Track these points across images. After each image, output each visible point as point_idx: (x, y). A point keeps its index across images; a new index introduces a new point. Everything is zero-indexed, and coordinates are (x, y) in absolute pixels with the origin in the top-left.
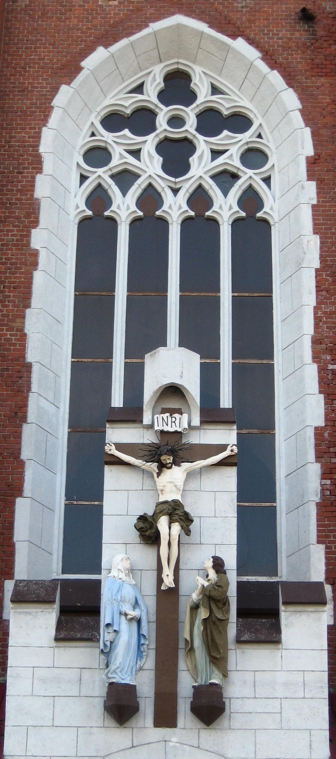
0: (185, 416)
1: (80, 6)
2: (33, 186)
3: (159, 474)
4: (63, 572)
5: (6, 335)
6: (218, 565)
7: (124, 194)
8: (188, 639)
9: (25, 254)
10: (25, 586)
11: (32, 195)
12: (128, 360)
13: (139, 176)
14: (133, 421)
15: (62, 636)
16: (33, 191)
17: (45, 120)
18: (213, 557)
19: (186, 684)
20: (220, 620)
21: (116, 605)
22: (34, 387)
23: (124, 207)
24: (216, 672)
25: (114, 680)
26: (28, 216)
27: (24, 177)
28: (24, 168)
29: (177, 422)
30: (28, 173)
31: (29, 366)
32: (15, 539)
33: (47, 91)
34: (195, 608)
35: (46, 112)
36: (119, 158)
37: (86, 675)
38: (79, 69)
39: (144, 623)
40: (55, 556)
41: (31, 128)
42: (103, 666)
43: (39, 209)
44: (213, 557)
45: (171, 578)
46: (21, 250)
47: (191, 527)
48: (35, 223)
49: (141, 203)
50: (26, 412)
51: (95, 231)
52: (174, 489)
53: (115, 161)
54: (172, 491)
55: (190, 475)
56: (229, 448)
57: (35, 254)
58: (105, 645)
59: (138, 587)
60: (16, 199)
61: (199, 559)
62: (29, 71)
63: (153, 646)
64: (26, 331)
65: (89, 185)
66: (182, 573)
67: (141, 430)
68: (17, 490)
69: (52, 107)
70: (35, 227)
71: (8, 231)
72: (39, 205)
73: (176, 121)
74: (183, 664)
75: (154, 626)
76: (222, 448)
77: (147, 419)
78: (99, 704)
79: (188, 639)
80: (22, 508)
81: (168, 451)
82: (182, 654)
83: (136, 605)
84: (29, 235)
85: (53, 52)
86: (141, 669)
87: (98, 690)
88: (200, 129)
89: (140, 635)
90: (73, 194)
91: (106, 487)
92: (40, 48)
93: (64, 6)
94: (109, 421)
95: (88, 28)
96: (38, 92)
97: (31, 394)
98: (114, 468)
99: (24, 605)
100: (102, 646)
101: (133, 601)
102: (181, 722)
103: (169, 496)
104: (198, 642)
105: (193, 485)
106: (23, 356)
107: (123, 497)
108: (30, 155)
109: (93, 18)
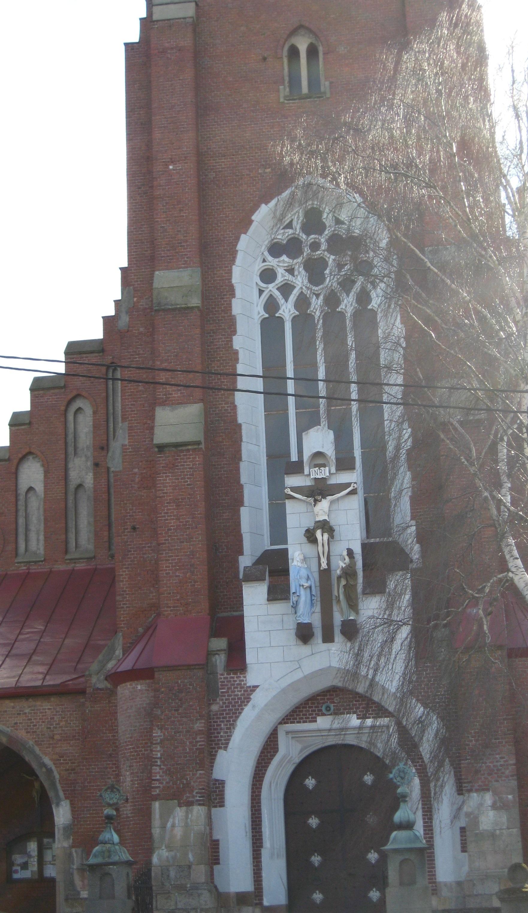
0: (327, 468)
1: (247, 175)
2: (231, 307)
3: (315, 505)
4: (271, 545)
5: (225, 407)
6: (350, 553)
7: (286, 301)
8: (337, 595)
9: (230, 353)
10: (249, 570)
11: (231, 313)
12: (298, 411)
13: (295, 287)
14: (300, 473)
15: (271, 598)
16: (231, 310)
17: (233, 261)
18: (347, 549)
19: (338, 619)
20: (352, 585)
21: (297, 581)
22: (244, 439)
23: (287, 310)
24: (353, 612)
25: (299, 621)
26: (230, 328)
27: (225, 301)
28: (224, 295)
29: (323, 472)
30: (227, 298)
31: (240, 426)
32: (242, 532)
33: (233, 240)
34: (339, 578)
35: (234, 254)
36: (282, 276)
37: (285, 618)
38: (251, 222)
39: (313, 588)
40: (265, 536)
41: (226, 267)
42: (293, 612)
43: (236, 322)
44: (347, 549)
45: (326, 562)
46: (228, 350)
47: (334, 534)
48: (234, 332)
49: (297, 306)
50: (241, 454)
51: (271, 326)
52: (323, 513)
53: (280, 279)
54: (322, 515)
55: (332, 502)
56: (352, 485)
57: (236, 353)
58: (293, 603)
59: (309, 568)
60: (222, 317)
61: (340, 549)
62: (220, 226)
63: (319, 599)
64: (236, 403)
65: (265, 296)
66: (331, 558)
67: (304, 477)
68: (240, 502)
69: (237, 251)
70: (235, 335)
71: (219, 339)
72: (235, 319)
73: (315, 246)
74: (335, 608)
75: (318, 588)
76: (348, 485)
77: (306, 471)
78: (293, 632)
79: (337, 595)
80: (245, 513)
81: (319, 491)
82: (334, 603)
83: (308, 578)
84: (231, 341)
85: (233, 210)
86: (314, 612)
87: (291, 625)
88: (330, 250)
89: (311, 595)
90: (255, 305)
91: (287, 512)
92: (225, 208)
93: (237, 176)
94: (287, 474)
95: (254, 191)
96: (227, 240)
97: (242, 443)
98: (291, 501)
99: (249, 583)
100: (292, 604)
101: (306, 577)
102: (336, 639)
103: (321, 518)
104: (342, 597)
105: (335, 507)
106: (236, 420)
107: (298, 516)
108: (226, 285)
109: (256, 183)
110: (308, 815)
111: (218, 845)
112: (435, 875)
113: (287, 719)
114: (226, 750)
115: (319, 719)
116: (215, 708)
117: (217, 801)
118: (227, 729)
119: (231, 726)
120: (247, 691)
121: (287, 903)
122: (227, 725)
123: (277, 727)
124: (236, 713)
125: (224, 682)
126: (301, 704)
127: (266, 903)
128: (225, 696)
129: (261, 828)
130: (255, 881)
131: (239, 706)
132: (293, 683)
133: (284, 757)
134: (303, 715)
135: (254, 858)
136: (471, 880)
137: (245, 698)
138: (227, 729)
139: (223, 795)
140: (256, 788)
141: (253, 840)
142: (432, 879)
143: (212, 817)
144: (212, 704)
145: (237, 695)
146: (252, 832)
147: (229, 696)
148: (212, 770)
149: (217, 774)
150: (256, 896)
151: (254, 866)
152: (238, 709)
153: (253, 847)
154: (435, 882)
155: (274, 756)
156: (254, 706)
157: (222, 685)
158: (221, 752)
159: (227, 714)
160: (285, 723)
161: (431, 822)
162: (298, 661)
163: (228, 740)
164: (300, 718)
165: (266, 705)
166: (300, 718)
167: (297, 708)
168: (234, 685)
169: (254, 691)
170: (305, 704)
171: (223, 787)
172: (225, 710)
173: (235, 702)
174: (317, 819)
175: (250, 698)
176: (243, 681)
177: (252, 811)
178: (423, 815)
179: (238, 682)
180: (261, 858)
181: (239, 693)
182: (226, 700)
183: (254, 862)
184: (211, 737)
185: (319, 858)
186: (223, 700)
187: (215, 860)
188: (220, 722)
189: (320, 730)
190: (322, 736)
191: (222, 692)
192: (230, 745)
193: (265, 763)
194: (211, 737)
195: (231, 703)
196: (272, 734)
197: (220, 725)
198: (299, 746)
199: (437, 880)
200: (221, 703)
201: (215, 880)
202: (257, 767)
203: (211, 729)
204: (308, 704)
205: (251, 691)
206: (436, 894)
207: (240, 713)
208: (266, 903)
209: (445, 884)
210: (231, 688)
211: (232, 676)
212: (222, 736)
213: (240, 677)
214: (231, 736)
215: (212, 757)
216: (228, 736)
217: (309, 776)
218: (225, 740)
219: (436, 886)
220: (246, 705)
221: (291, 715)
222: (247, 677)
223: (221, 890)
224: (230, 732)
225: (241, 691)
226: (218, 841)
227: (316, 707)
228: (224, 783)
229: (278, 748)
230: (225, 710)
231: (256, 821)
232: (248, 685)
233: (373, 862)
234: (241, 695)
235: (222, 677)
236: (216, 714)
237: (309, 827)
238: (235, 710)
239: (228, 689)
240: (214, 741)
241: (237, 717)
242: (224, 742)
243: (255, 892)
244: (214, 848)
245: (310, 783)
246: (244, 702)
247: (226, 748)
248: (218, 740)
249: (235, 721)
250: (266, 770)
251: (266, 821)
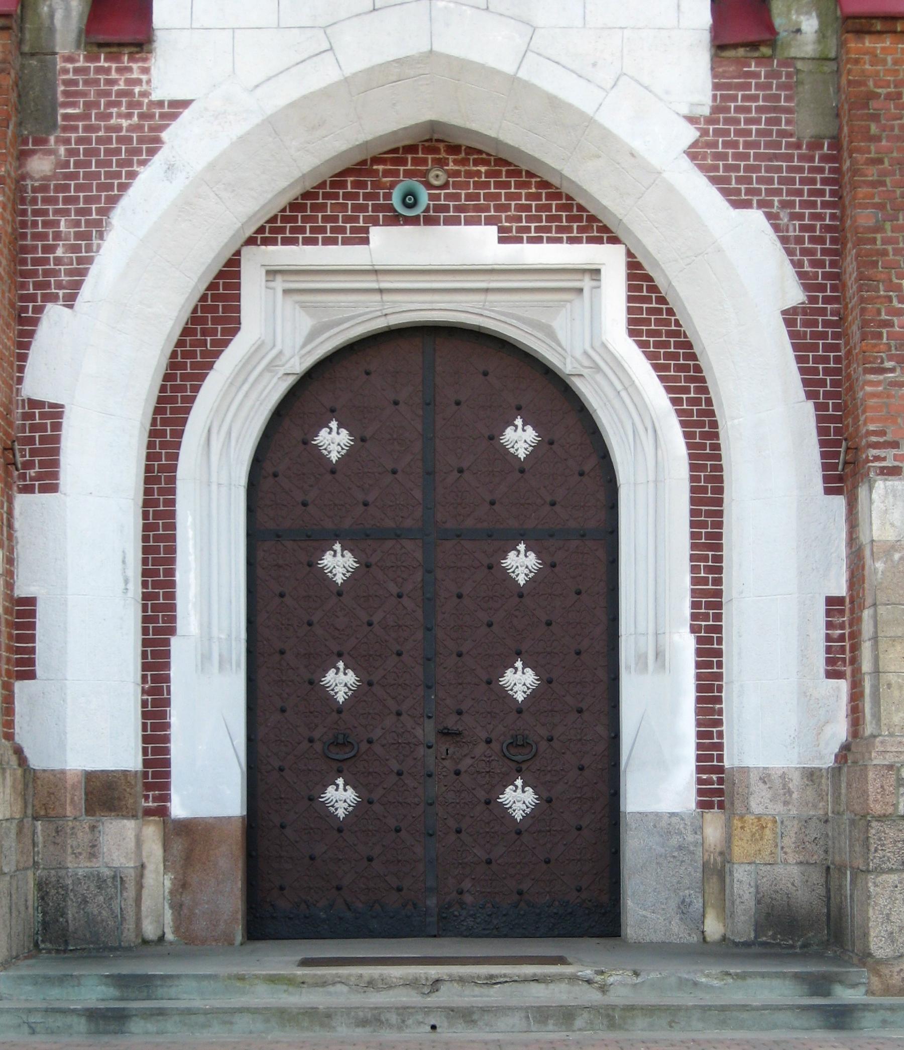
110: (323, 540)
111: (33, 613)
112: (719, 747)
113: (273, 230)
114: (71, 307)
115: (376, 233)
116: (40, 166)
117: (32, 472)
118: (79, 236)
119: (92, 230)
120: (151, 116)
121: (245, 813)
122: (77, 224)
123: (238, 253)
124: (110, 187)
125: (75, 83)
126: (322, 185)
127: (178, 809)
128: (75, 129)
129: (171, 573)
130: (146, 739)
131: (120, 164)
132: (305, 97)
133: (259, 348)
134: (326, 219)
135: (145, 667)
136: (890, 767)
137: (141, 140)
138: (79, 236)
139: (56, 451)
140: (163, 445)
141: (145, 608)
142: (710, 758)
143: (17, 525)
144: (32, 152)
145: (118, 128)
146: (145, 584)
147: (88, 129)
148: (21, 369)
149: (40, 381)
150: (148, 787)
151: (144, 692)
152: (118, 175)
153: (145, 631)
154: (720, 770)
155: (226, 344)
156: (170, 168)
157: (66, 94)
158: (54, 313)
159: (78, 188)
160: (266, 242)
161: (718, 581)
162: (325, 28)
163: (79, 273)
164: (313, 230)
165: (212, 167)
166: (313, 230)
167: (306, 195)
168: (107, 94)
169: (174, 116)
170: (334, 184)
171: (57, 427)
172: (74, 176)
173: (108, 152)
174: (348, 554)
175: (158, 140)
176: (139, 82)
177: (145, 515)
178: (693, 558)
179: (122, 86)
180: (167, 666)
181: (125, 123)
182: (79, 141)
183: (144, 679)
184: (24, 262)
185: (351, 678)
186: (67, 141)
187: (19, 662)
188: (57, 212)
189: (376, 272)
190: (381, 291)
191: (66, 117)
192: (86, 291)
193: (194, 366)
194: (24, 262)
195: (95, 152)
196: (221, 275)
197: (56, 224)
198: (306, 323)
199: (727, 764)
200: (62, 150)
201: (17, 729)
202: (167, 377)
203: (24, 236)
204: (343, 185)
205: (163, 116)
206: (721, 806)
207: (124, 187)
208: (178, 809)
209: (765, 777)
210: (97, 104)
211: (102, 63)
212: (58, 261)
213: (129, 70)
214: (90, 261)
215: (25, 326)
216: (80, 261)
217: (330, 420)
218: (69, 273)
219: (721, 781)
220: (143, 163)
221: (285, 219)
222: (153, 71)
223: (36, 762)
224: (89, 248)
225: (129, 116)
226: (31, 601)
227: (367, 197)
228: (60, 415)
229: (238, 321)
230: (74, 176)
231: (156, 550)
232: (155, 97)
233: (520, 697)
234: (131, 128)
235: (70, 66)
236: (44, 188)
237: (323, 578)
238: (109, 175)
239: (88, 105)
240: (34, 273)
241: (113, 200)
242: (64, 278)
243: (145, 775)
244: (18, 626)
245: (334, 441)
246: (138, 152)
247: (70, 301)
248: (47, 273)
249: (105, 212)
250: (196, 389)
251: (191, 550)
